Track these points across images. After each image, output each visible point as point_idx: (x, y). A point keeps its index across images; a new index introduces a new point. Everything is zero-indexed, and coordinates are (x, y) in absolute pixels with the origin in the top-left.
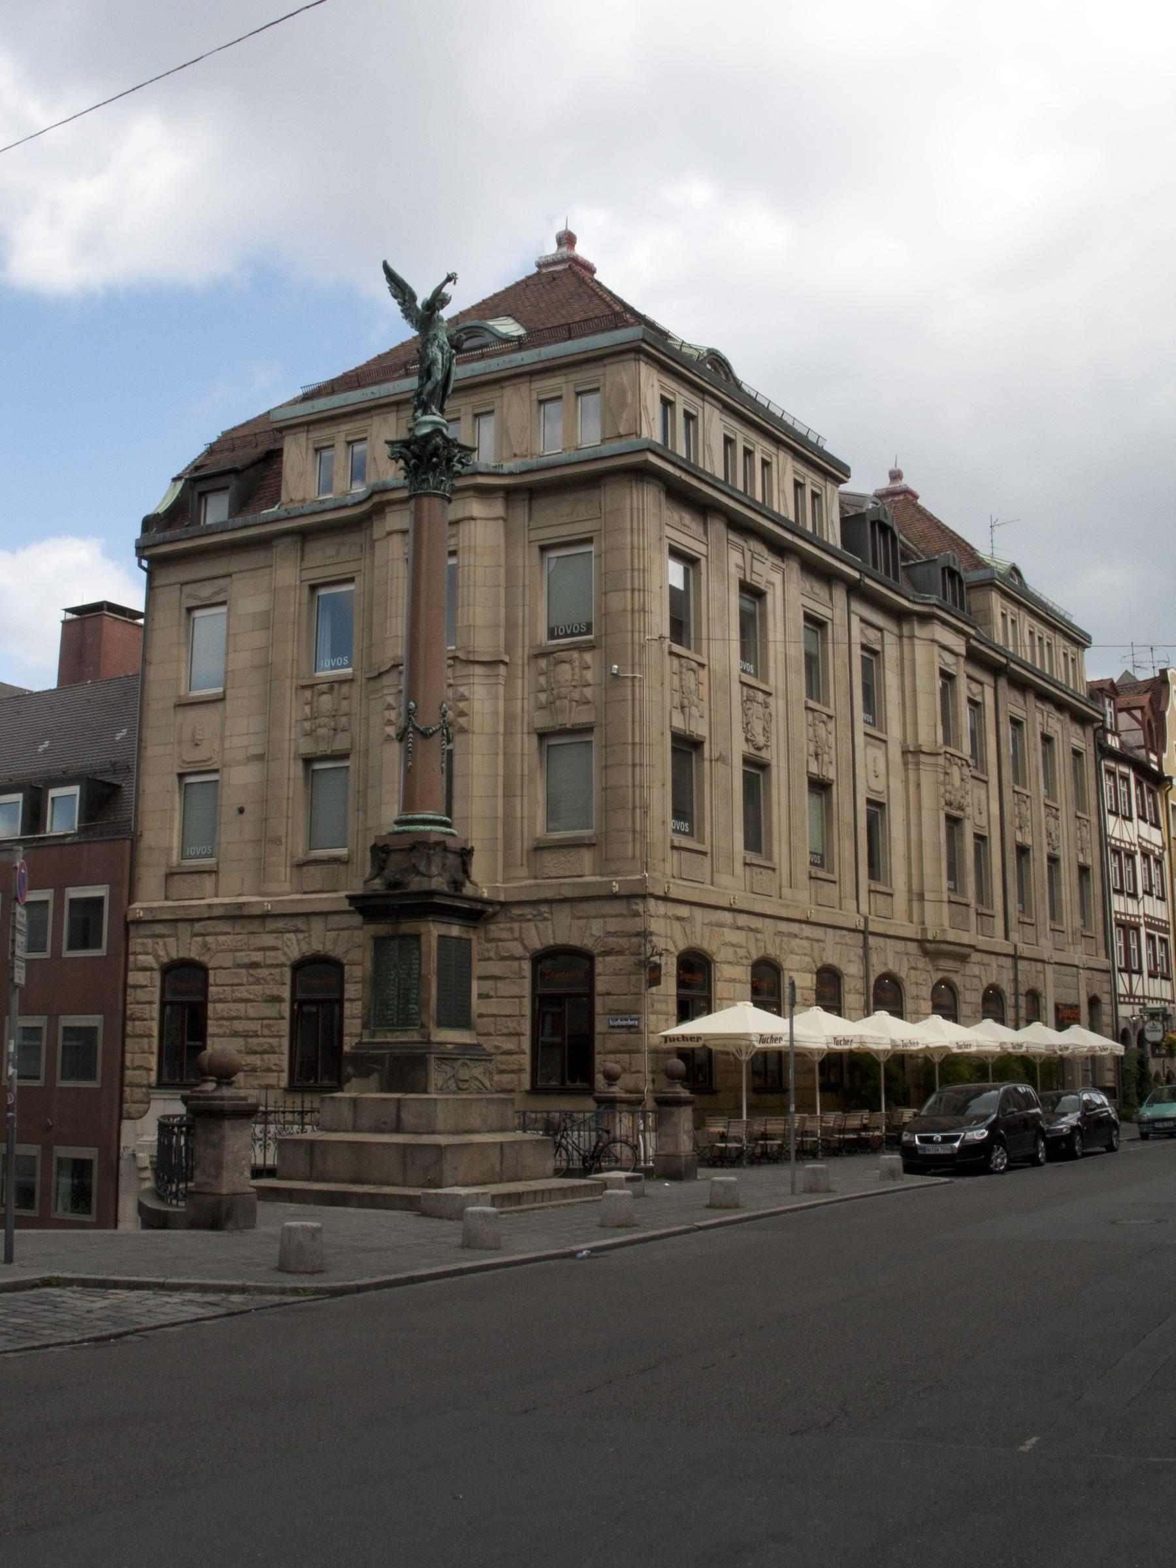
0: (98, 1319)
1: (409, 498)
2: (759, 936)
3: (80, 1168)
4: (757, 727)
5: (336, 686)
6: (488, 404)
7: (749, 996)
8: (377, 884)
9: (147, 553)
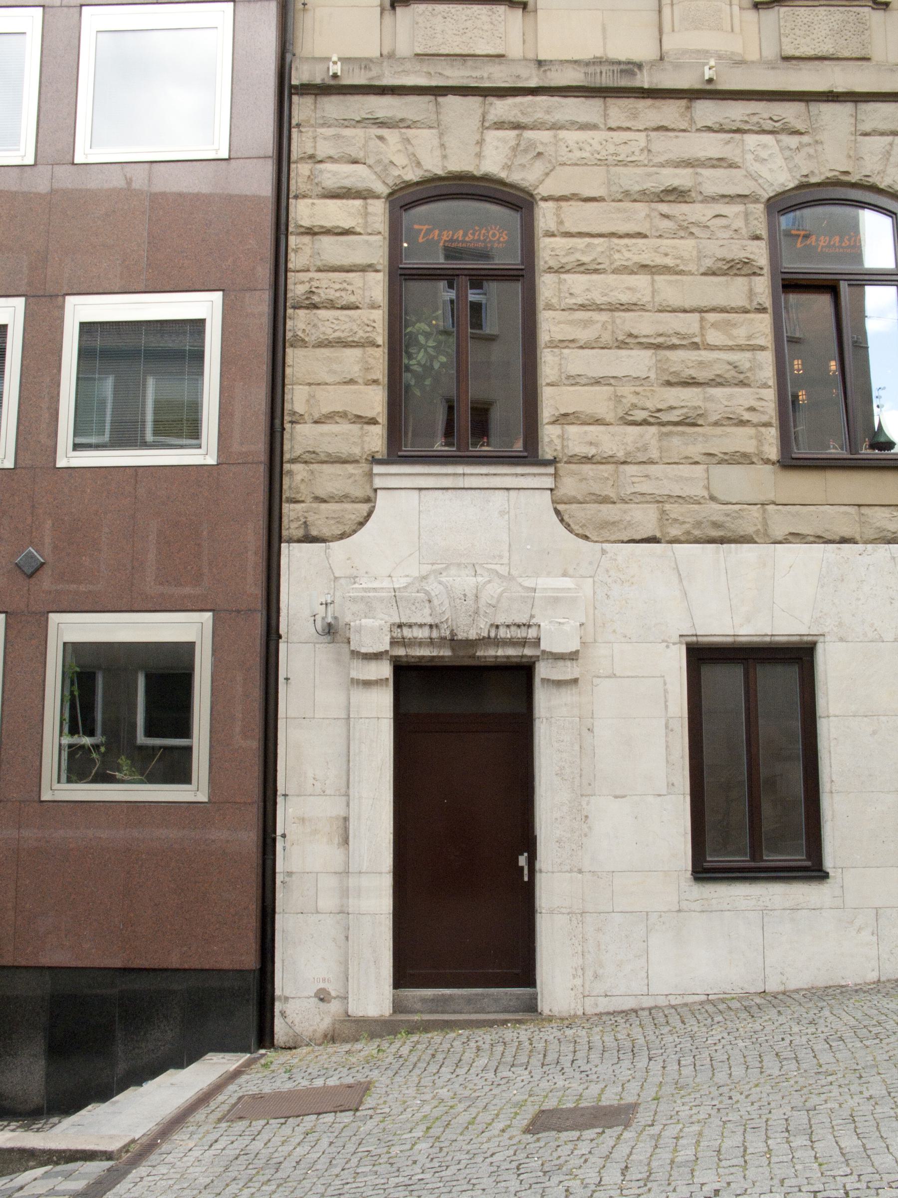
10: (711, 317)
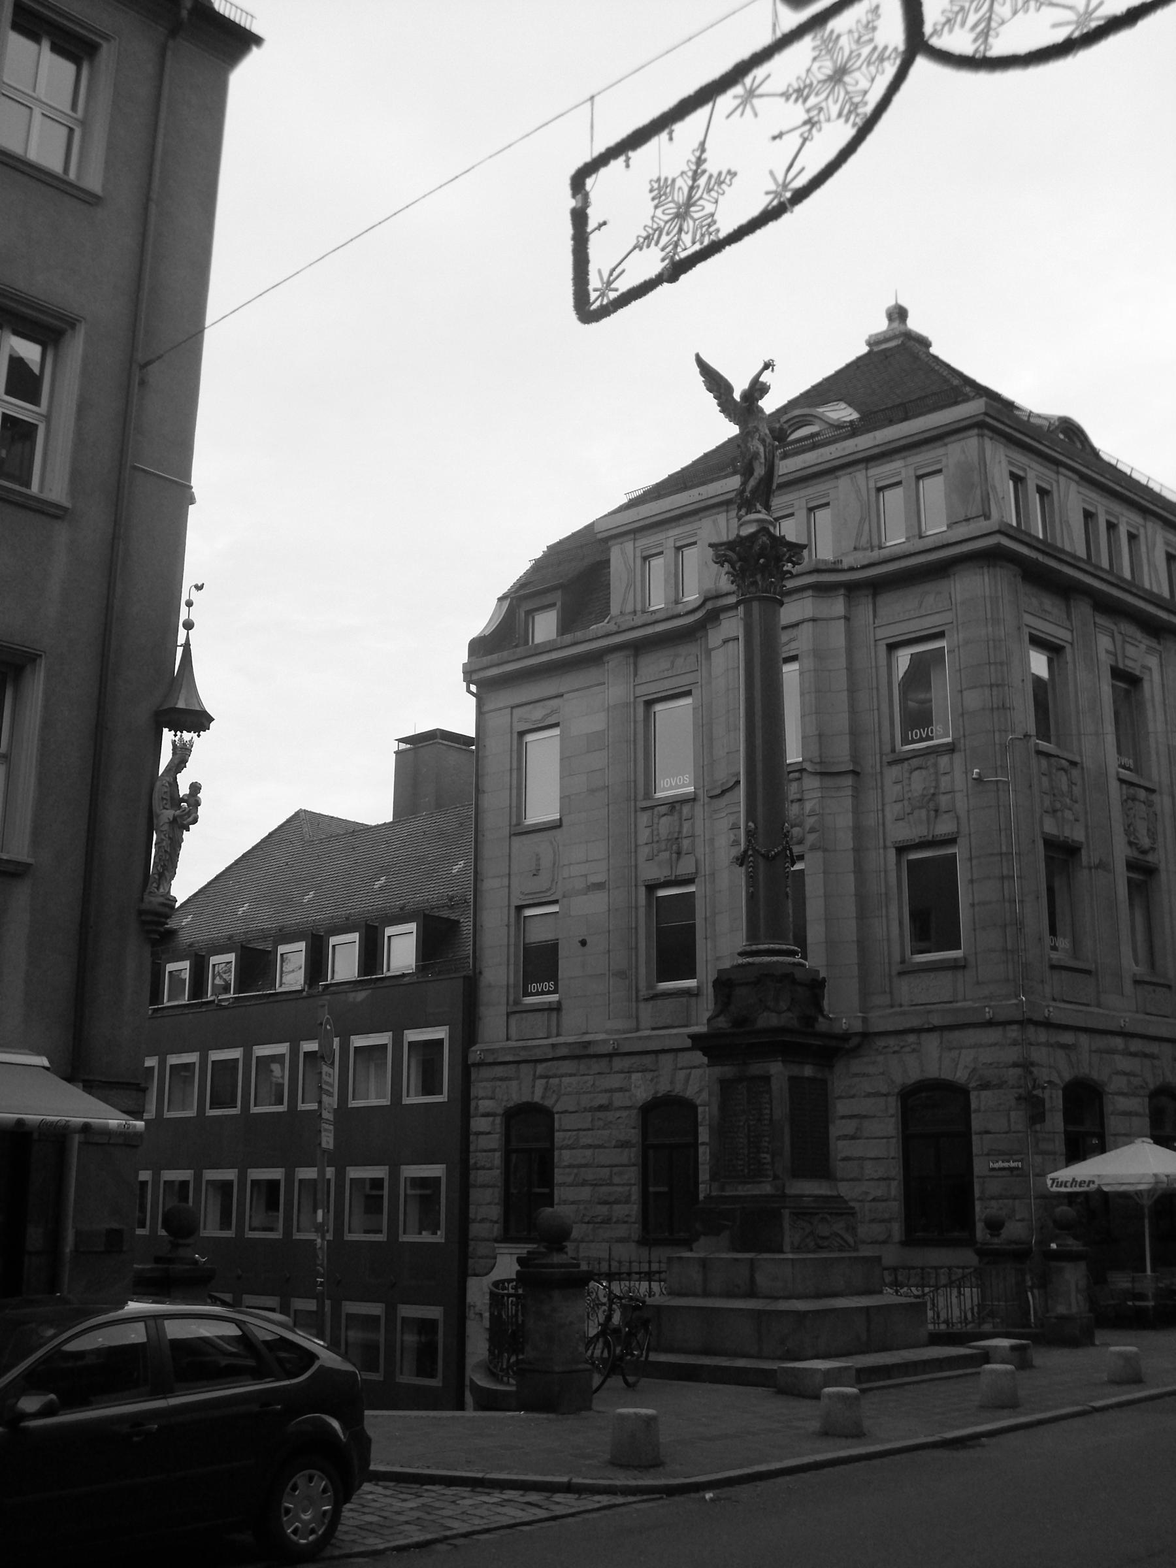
0: (407, 1523)
1: (738, 603)
2: (1156, 1062)
3: (426, 1327)
4: (1142, 828)
5: (678, 806)
6: (824, 496)
7: (1148, 1131)
8: (722, 1023)
9: (475, 677)
10: (615, 1169)
